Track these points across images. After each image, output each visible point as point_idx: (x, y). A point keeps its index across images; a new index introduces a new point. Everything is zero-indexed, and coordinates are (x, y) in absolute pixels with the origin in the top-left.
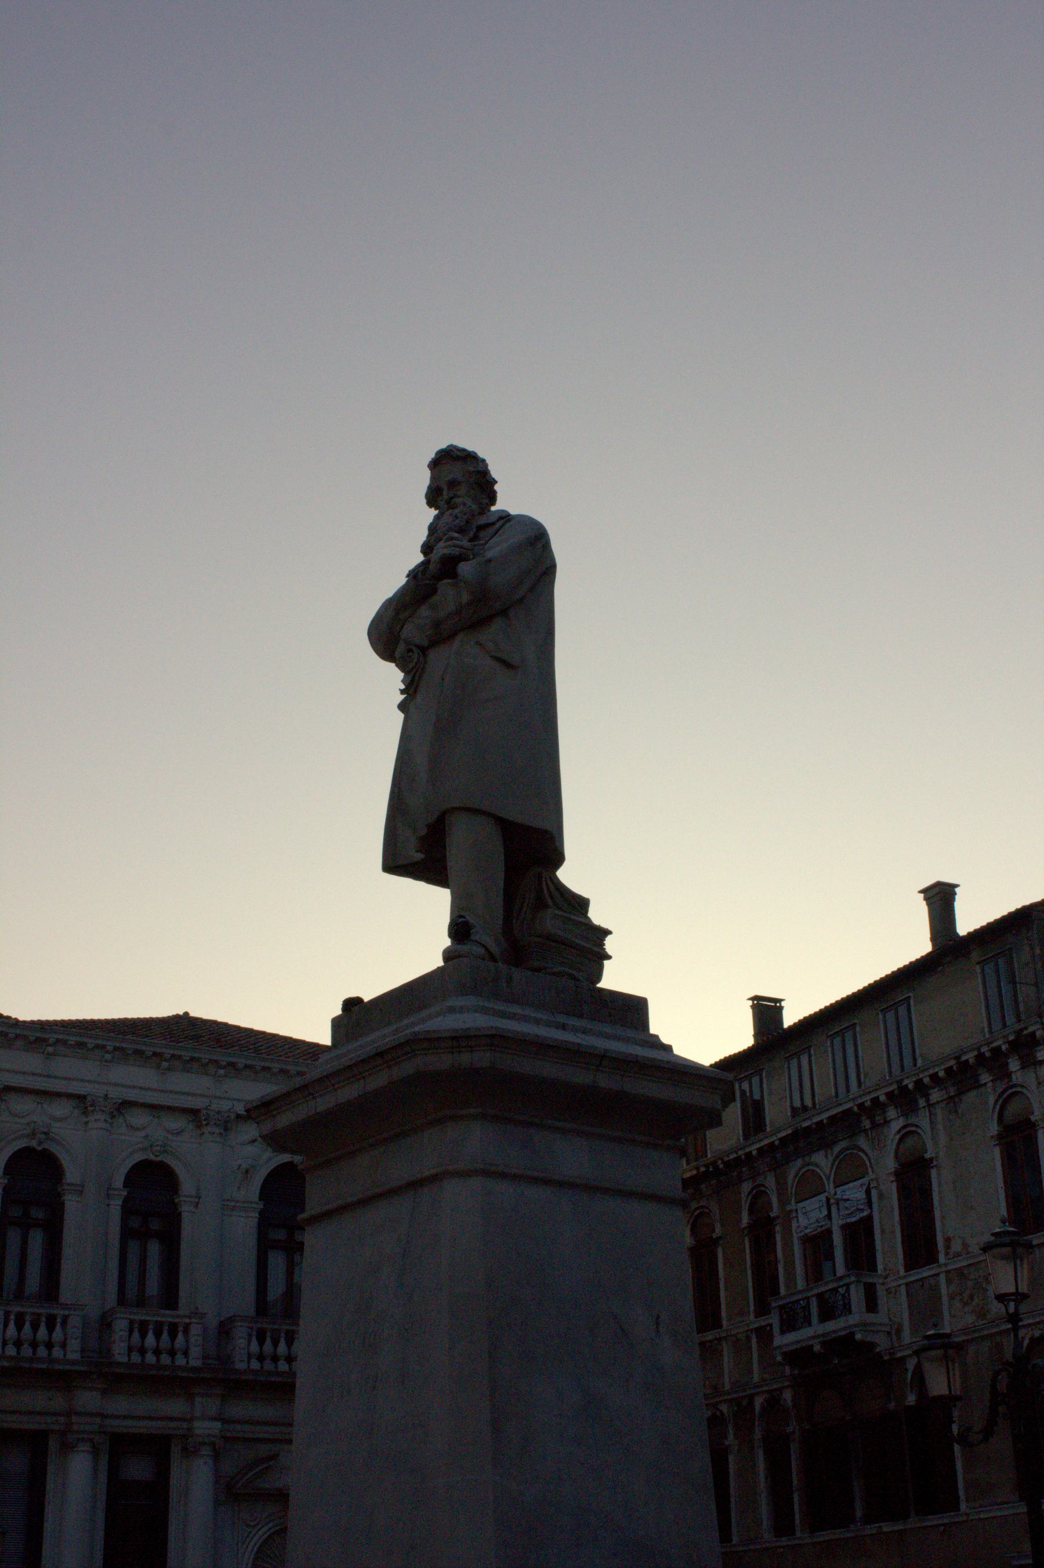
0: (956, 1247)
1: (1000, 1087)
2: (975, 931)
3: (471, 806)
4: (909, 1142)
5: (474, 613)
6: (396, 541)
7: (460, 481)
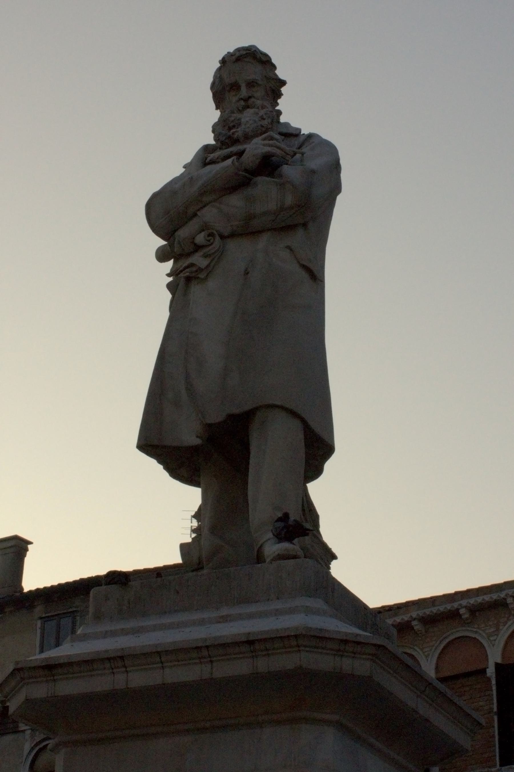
2: (45, 588)
3: (287, 406)
5: (248, 213)
6: (191, 126)
7: (246, 82)
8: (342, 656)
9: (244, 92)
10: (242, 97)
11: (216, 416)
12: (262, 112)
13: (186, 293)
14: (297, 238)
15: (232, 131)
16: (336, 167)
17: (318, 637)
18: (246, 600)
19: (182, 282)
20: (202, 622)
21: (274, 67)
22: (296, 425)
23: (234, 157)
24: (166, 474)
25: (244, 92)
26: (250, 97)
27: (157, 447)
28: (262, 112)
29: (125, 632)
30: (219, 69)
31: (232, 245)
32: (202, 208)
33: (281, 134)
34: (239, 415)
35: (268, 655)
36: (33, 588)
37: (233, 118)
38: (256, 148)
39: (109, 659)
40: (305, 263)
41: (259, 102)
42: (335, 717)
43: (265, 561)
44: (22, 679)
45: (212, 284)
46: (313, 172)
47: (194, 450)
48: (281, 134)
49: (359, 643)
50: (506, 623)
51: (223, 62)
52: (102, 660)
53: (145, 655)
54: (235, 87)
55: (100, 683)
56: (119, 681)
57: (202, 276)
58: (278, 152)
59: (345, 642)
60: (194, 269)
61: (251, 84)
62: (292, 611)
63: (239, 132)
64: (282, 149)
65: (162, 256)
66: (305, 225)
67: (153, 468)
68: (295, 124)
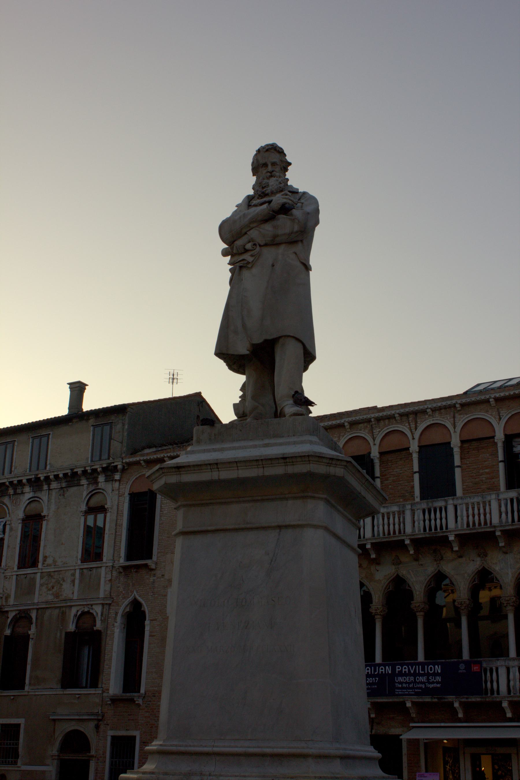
0: (49, 561)
1: (92, 488)
4: (33, 505)
7: (270, 162)
8: (330, 466)
9: (270, 168)
10: (269, 170)
11: (258, 340)
12: (280, 180)
13: (240, 274)
14: (298, 248)
15: (265, 189)
16: (317, 211)
17: (319, 457)
18: (276, 436)
19: (238, 268)
20: (255, 446)
21: (285, 155)
22: (300, 345)
23: (267, 204)
24: (227, 367)
25: (270, 168)
26: (273, 171)
27: (224, 354)
28: (280, 180)
29: (214, 450)
30: (256, 155)
31: (266, 251)
32: (250, 230)
33: (290, 192)
34: (266, 339)
35: (293, 465)
36: (89, 409)
37: (264, 182)
38: (278, 200)
39: (210, 464)
40: (303, 261)
41: (277, 174)
42: (325, 496)
43: (285, 416)
44: (163, 473)
45: (254, 271)
46: (308, 213)
47: (242, 357)
48: (290, 192)
49: (339, 460)
50: (344, 436)
51: (259, 151)
52: (206, 465)
53: (229, 463)
54: (265, 165)
55: (205, 476)
56: (215, 475)
57: (250, 266)
58: (290, 202)
59: (332, 459)
60: (245, 262)
61: (274, 164)
62: (302, 442)
63: (268, 190)
64: (291, 200)
65: (225, 253)
66: (302, 241)
67: (221, 364)
68: (295, 186)
